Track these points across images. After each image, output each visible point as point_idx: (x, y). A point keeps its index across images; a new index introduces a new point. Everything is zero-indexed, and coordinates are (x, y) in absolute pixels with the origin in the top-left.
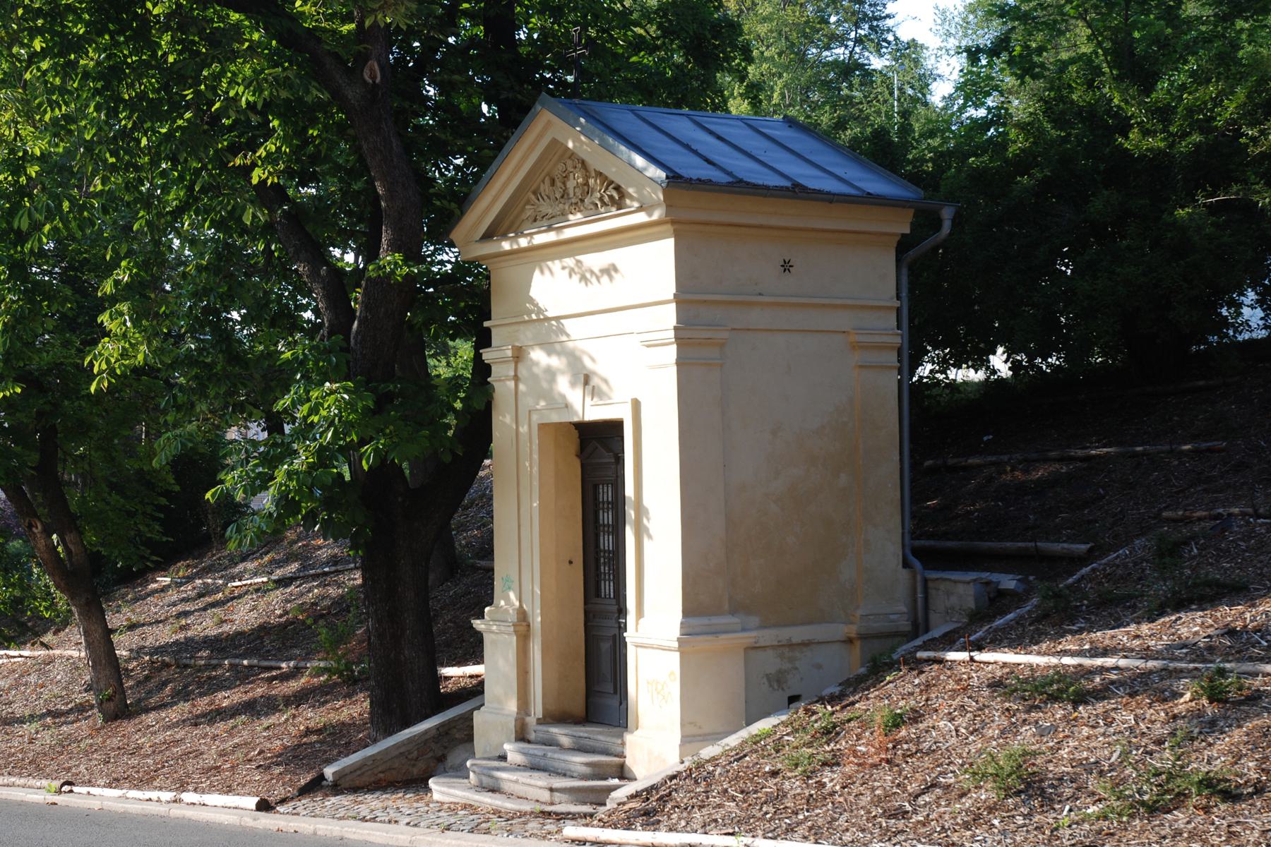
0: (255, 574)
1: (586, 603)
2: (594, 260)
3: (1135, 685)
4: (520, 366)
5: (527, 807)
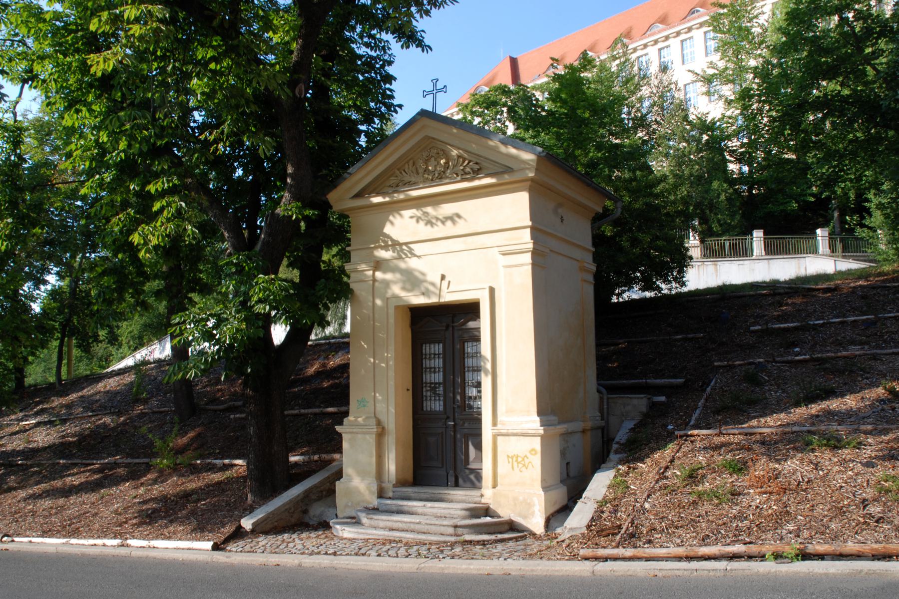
2: (448, 209)
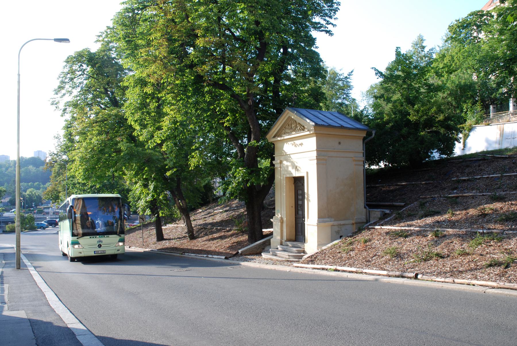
0: (220, 209)
1: (295, 215)
2: (298, 142)
3: (419, 234)
4: (281, 165)
5: (284, 259)
